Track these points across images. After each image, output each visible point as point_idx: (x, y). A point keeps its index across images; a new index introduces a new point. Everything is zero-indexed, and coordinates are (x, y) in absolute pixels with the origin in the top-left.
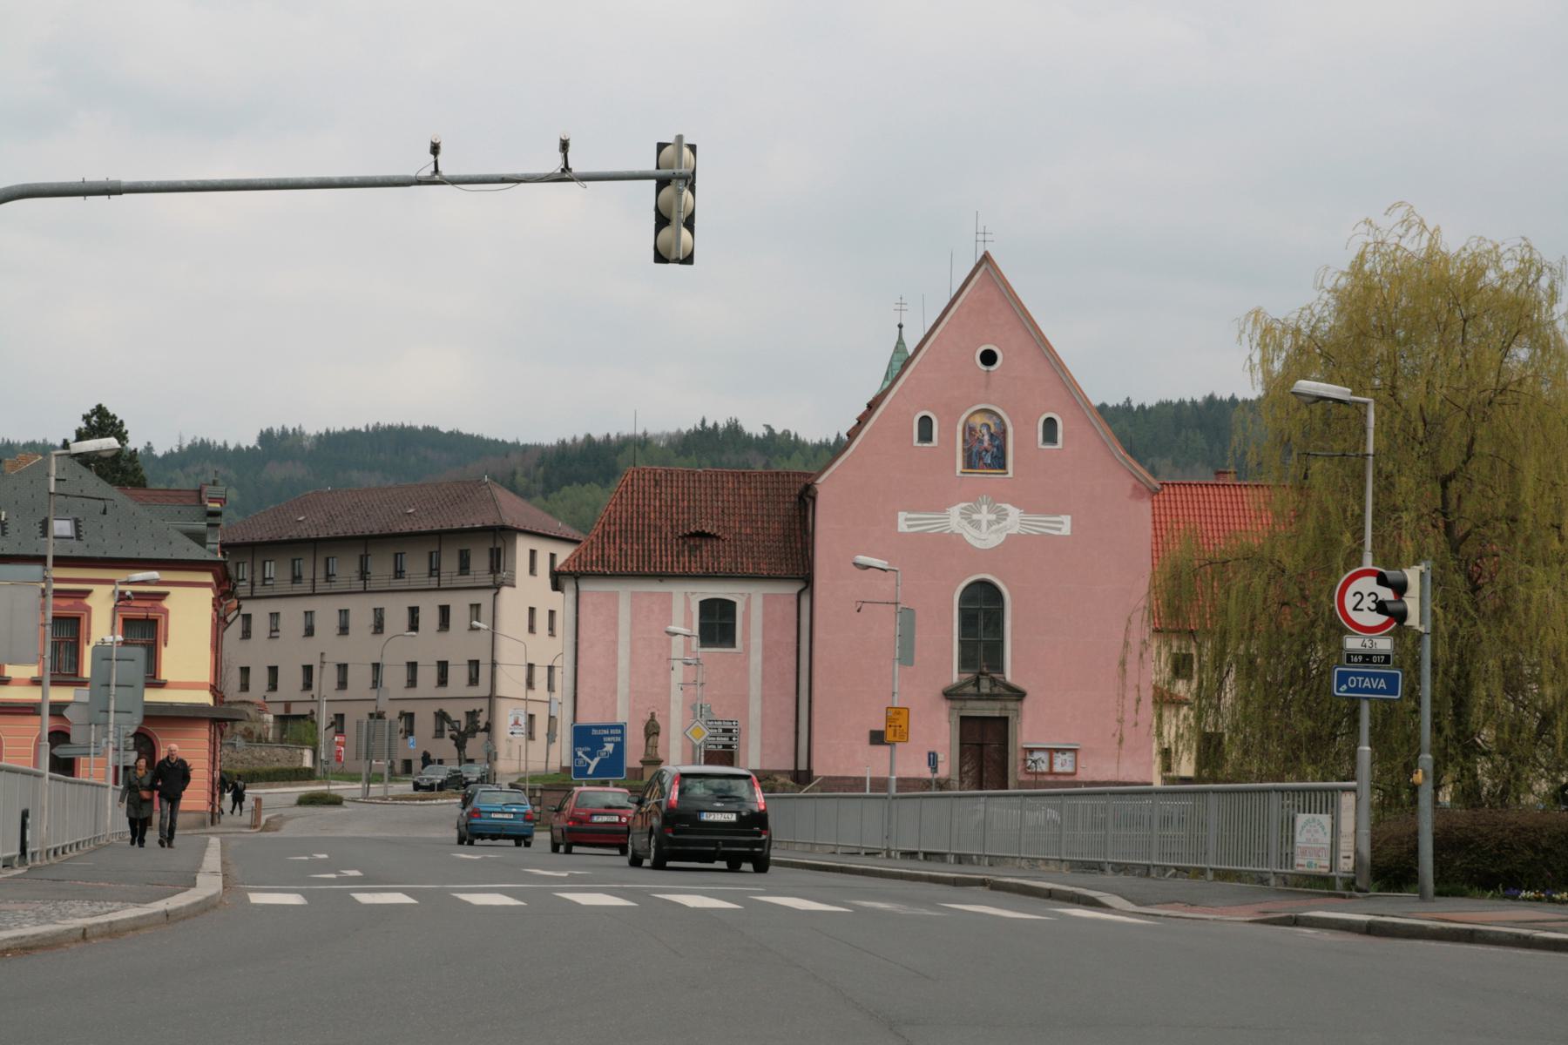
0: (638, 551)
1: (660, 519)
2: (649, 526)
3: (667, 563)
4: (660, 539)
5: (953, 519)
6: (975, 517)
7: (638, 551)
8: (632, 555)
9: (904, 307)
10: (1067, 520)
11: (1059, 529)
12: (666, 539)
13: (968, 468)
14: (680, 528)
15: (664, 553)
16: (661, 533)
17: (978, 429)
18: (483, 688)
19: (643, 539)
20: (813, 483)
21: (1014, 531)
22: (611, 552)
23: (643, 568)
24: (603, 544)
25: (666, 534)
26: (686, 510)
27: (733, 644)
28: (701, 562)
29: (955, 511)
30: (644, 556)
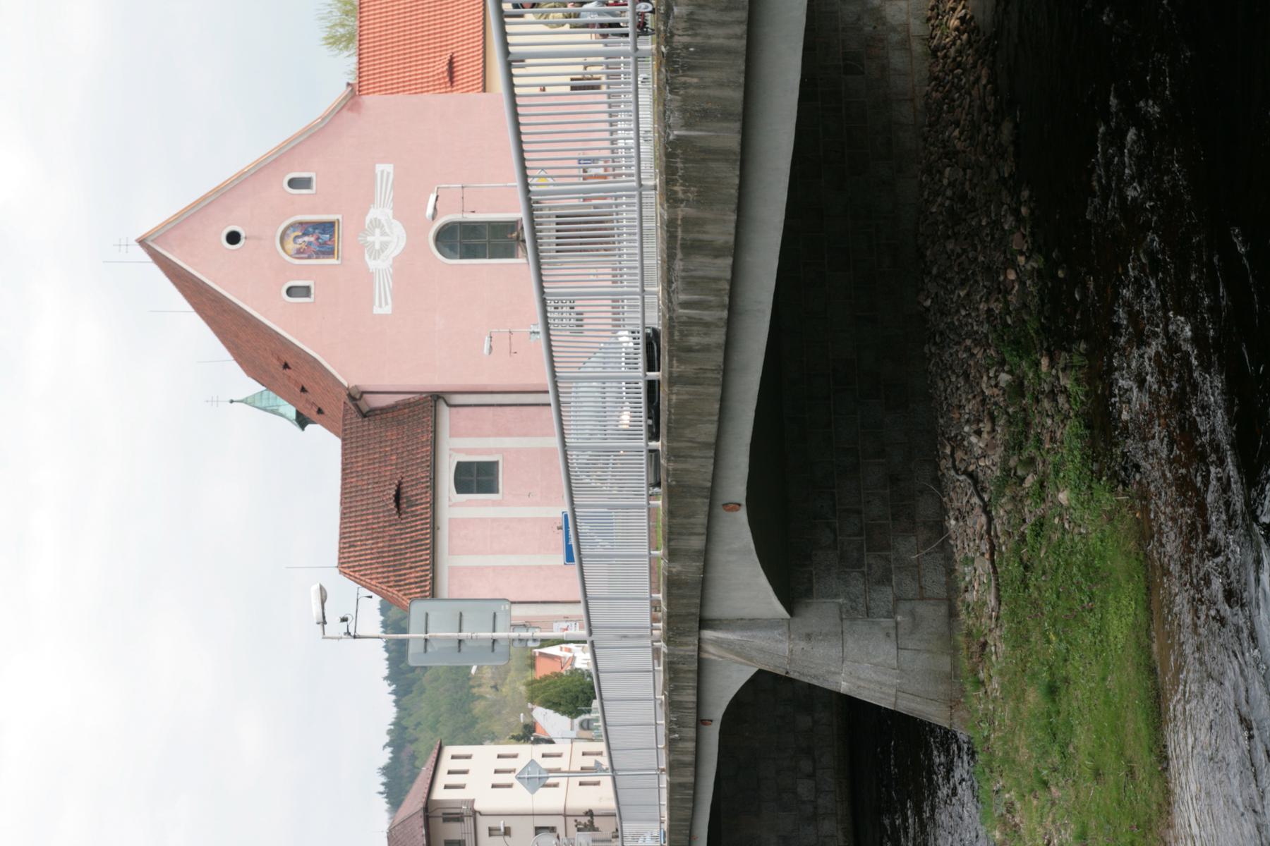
0: (412, 552)
1: (384, 537)
2: (390, 546)
3: (422, 524)
4: (401, 534)
5: (380, 265)
6: (377, 247)
7: (412, 552)
8: (416, 557)
9: (215, 399)
10: (379, 167)
11: (388, 174)
12: (401, 529)
13: (333, 254)
14: (392, 518)
15: (413, 529)
16: (395, 535)
17: (298, 246)
18: (558, 822)
19: (401, 549)
20: (348, 389)
21: (390, 212)
22: (413, 576)
23: (427, 544)
24: (406, 584)
25: (397, 530)
26: (376, 516)
27: (495, 464)
28: (422, 493)
29: (372, 264)
30: (417, 546)
